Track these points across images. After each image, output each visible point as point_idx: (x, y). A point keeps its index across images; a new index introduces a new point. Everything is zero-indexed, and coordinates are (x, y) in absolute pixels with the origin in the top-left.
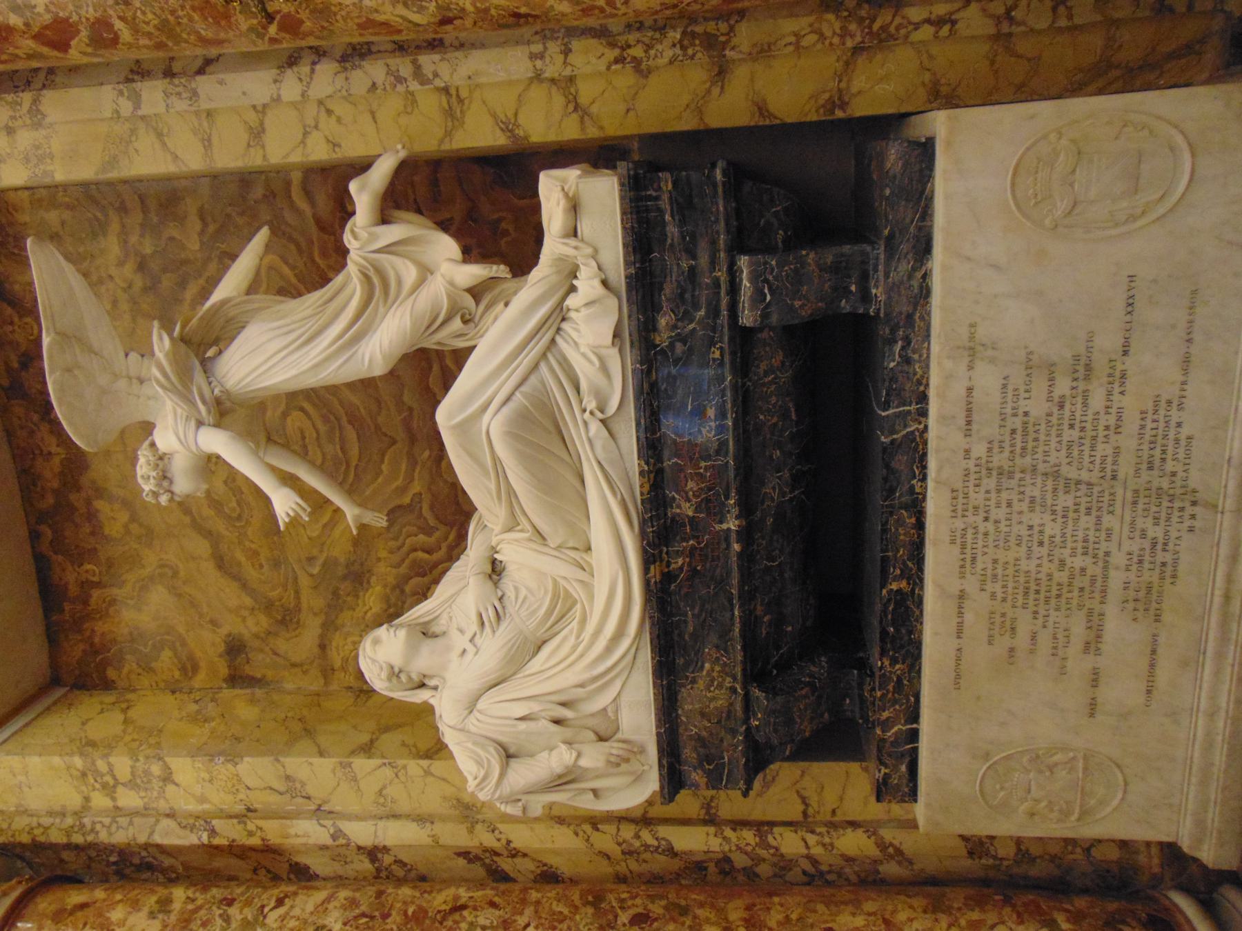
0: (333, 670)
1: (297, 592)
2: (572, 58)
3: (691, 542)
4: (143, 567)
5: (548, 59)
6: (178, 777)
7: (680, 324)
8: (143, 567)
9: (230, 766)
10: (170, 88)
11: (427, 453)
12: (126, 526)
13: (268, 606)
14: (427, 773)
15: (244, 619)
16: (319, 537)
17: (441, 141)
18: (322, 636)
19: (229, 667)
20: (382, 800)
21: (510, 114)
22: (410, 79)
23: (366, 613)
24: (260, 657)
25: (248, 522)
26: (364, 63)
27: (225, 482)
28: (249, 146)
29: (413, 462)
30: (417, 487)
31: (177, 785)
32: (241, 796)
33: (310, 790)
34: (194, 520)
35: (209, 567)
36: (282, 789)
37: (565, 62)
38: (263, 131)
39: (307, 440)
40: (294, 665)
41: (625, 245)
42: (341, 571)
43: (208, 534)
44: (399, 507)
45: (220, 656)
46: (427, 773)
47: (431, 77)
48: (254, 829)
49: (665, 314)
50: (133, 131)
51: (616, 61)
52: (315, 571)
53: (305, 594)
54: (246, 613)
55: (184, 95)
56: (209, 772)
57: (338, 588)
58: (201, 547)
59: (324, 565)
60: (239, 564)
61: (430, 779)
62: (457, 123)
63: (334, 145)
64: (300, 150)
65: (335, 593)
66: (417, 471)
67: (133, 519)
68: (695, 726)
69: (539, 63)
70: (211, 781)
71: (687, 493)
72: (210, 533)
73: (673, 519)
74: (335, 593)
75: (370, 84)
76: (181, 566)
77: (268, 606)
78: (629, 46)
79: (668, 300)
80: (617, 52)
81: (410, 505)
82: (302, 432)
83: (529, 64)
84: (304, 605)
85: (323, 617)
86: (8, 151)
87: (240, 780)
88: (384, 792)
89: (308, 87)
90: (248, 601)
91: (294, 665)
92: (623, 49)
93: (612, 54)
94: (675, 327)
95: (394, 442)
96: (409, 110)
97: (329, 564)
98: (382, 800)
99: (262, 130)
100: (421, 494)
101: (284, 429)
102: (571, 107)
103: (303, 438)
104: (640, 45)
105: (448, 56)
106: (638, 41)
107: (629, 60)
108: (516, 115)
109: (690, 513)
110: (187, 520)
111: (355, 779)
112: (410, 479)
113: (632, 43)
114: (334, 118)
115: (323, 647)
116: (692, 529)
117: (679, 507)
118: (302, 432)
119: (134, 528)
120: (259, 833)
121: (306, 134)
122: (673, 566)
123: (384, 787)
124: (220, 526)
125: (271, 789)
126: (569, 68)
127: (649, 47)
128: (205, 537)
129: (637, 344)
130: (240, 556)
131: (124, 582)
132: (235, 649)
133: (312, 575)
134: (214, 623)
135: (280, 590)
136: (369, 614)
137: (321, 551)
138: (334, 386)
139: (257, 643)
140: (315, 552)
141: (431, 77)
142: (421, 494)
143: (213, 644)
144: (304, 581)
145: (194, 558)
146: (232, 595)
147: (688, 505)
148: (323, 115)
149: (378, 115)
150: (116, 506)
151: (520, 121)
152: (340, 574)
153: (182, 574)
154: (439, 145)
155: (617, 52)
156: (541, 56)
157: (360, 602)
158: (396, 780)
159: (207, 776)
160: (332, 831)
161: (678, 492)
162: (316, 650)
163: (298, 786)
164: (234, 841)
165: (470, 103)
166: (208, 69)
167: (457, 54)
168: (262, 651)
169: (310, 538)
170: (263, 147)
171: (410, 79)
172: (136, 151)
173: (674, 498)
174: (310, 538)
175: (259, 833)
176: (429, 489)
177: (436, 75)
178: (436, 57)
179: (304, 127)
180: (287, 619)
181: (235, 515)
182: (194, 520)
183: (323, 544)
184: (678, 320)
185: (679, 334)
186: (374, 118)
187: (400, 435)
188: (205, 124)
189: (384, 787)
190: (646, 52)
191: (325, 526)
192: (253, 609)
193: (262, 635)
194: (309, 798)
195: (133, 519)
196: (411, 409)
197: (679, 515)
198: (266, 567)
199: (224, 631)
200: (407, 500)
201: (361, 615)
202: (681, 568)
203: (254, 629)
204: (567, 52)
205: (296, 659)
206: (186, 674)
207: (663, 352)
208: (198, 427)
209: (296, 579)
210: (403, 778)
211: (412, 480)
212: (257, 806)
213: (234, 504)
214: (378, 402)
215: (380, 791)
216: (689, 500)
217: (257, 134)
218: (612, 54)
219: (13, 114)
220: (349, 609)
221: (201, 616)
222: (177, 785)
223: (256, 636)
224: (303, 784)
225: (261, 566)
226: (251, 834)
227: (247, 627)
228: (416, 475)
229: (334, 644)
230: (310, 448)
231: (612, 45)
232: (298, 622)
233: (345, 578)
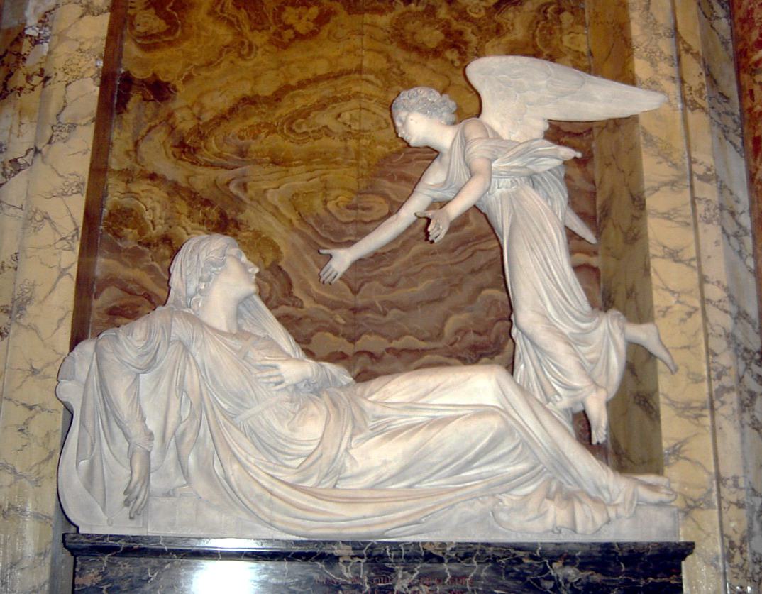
0: (128, 182)
1: (212, 165)
2: (734, 507)
3: (368, 587)
4: (252, 30)
5: (734, 490)
6: (88, 19)
7: (568, 585)
8: (252, 30)
9: (93, 72)
10: (712, 206)
11: (341, 321)
12: (291, 27)
13: (200, 133)
14: (63, 272)
15: (190, 108)
16: (266, 199)
17: (666, 396)
18: (164, 179)
19: (143, 81)
20: (38, 218)
21: (686, 454)
22: (720, 383)
23: (184, 228)
24: (149, 113)
25: (287, 137)
26: (731, 350)
27: (326, 127)
28: (664, 247)
29: (334, 306)
30: (308, 304)
31: (81, 17)
32: (61, 76)
33: (58, 146)
34: (293, 88)
35: (246, 89)
36: (63, 118)
37: (731, 503)
38: (676, 261)
39: (360, 212)
40: (136, 144)
41: (635, 544)
42: (230, 213)
43: (277, 98)
44: (290, 285)
45: (154, 75)
46: (63, 272)
47: (722, 399)
48: (33, 83)
49: (577, 574)
50: (675, 165)
51: (731, 543)
52: (233, 188)
53: (211, 173)
54: (196, 110)
55: (708, 213)
56: (89, 51)
57: (212, 206)
58: (266, 88)
59: (237, 197)
60: (246, 117)
61: (55, 273)
62: (680, 411)
63: (665, 312)
64: (661, 285)
65: (207, 202)
66: (326, 309)
67: (298, 36)
68: (157, 578)
69: (730, 482)
70: (80, 50)
71: (417, 585)
72: (278, 100)
73: (392, 570)
74: (207, 202)
75: (718, 352)
76: (250, 64)
77: (200, 133)
78: (741, 553)
79: (588, 577)
80: (738, 543)
81: (291, 294)
82: (369, 209)
83: (730, 475)
84: (199, 170)
85: (184, 185)
86: (661, 72)
87: (76, 78)
88: (46, 222)
89: (714, 305)
90: (207, 117)
91: (136, 144)
92: (741, 547)
93: (736, 539)
94: (566, 581)
95: (355, 292)
96: (691, 376)
97: (238, 204)
98: (38, 218)
99: (678, 261)
100: (302, 307)
101: (373, 193)
102: (691, 503)
103: (363, 209)
104: (743, 561)
105: (737, 415)
106: (745, 560)
107: (732, 552)
108: (685, 458)
109: (396, 588)
110: (293, 83)
111: (64, 194)
112: (319, 300)
113: (744, 556)
114: (685, 317)
115: (153, 177)
116: (380, 588)
117: (404, 577)
118: (369, 209)
119: (289, 34)
120: (28, 86)
121: (673, 292)
122: (344, 567)
123: (52, 223)
124: (284, 110)
125: (64, 107)
126: (727, 506)
127: (741, 568)
128: (275, 93)
129: (558, 548)
130: (254, 120)
131: (238, 8)
132: (159, 90)
133: (228, 184)
134: (189, 78)
135: (216, 149)
136: (183, 231)
137: (251, 199)
138: (362, 238)
139: (163, 113)
140: (251, 192)
141: (722, 399)
142: (302, 307)
143: (167, 72)
144: (223, 175)
145: (255, 78)
146: (218, 102)
147: (406, 586)
148: (688, 309)
149: (686, 350)
150: (311, 25)
151: (682, 462)
152: (228, 212)
153: (240, 62)
154: (663, 394)
155: (738, 543)
156: (736, 485)
157: (196, 225)
158: (58, 237)
159: (86, 47)
160: (20, 161)
161: (420, 577)
162: (150, 170)
163: (64, 135)
164: (24, 59)
165: (696, 425)
166: (725, 236)
167: (738, 422)
168: (155, 115)
169: (265, 191)
170: (663, 258)
171: (720, 383)
172: (660, 163)
173: (412, 573)
174: (265, 191)
175: (28, 86)
176: (306, 317)
177: (723, 403)
178: (736, 405)
179: (679, 293)
180: (185, 149)
181: (294, 127)
182: (293, 88)
183: (259, 202)
184: (572, 584)
185: (560, 585)
186: (685, 347)
187: (360, 301)
188: (680, 219)
189: (52, 223)
190: (737, 566)
191: (276, 208)
192: (199, 119)
193: (171, 121)
194: (49, 143)
195: (298, 36)
196: (385, 314)
197: (396, 576)
198: (240, 142)
199: (180, 87)
200: (297, 292)
201: (184, 224)
202: (341, 575)
203: (178, 115)
204: (740, 505)
205: (143, 147)
206: (139, 37)
207: (546, 570)
208: (488, 159)
209: (226, 168)
210: (59, 245)
211: (317, 302)
212: (48, 88)
213: (304, 129)
214: (393, 286)
215: (48, 218)
216: (410, 586)
217: (674, 256)
218: (736, 539)
219: (694, 89)
220: (190, 212)
221: (197, 68)
222: (81, 17)
223: (171, 115)
224: (65, 140)
225: (242, 138)
226: (29, 78)
227: (181, 108)
228: (321, 307)
229: (156, 189)
230: (353, 212)
231: (743, 540)
232: (181, 159)
233: (223, 215)
